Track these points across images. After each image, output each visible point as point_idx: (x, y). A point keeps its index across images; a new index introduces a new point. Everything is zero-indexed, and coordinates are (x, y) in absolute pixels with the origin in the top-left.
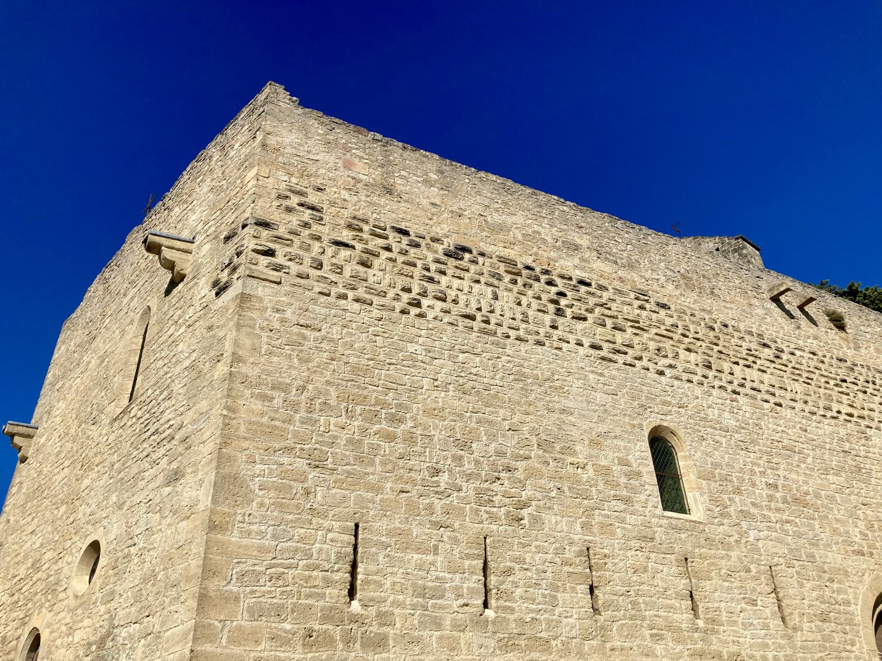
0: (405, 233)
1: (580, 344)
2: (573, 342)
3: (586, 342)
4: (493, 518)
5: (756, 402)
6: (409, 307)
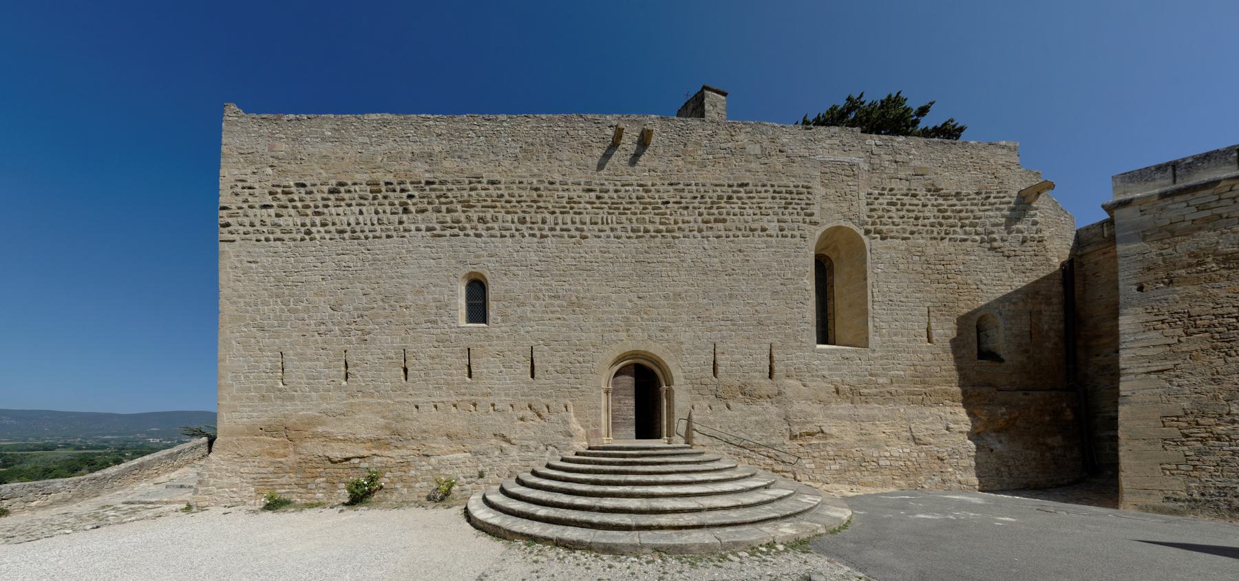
0: (303, 185)
1: (418, 230)
2: (247, 224)
3: (423, 227)
4: (350, 343)
5: (563, 239)
6: (945, 236)
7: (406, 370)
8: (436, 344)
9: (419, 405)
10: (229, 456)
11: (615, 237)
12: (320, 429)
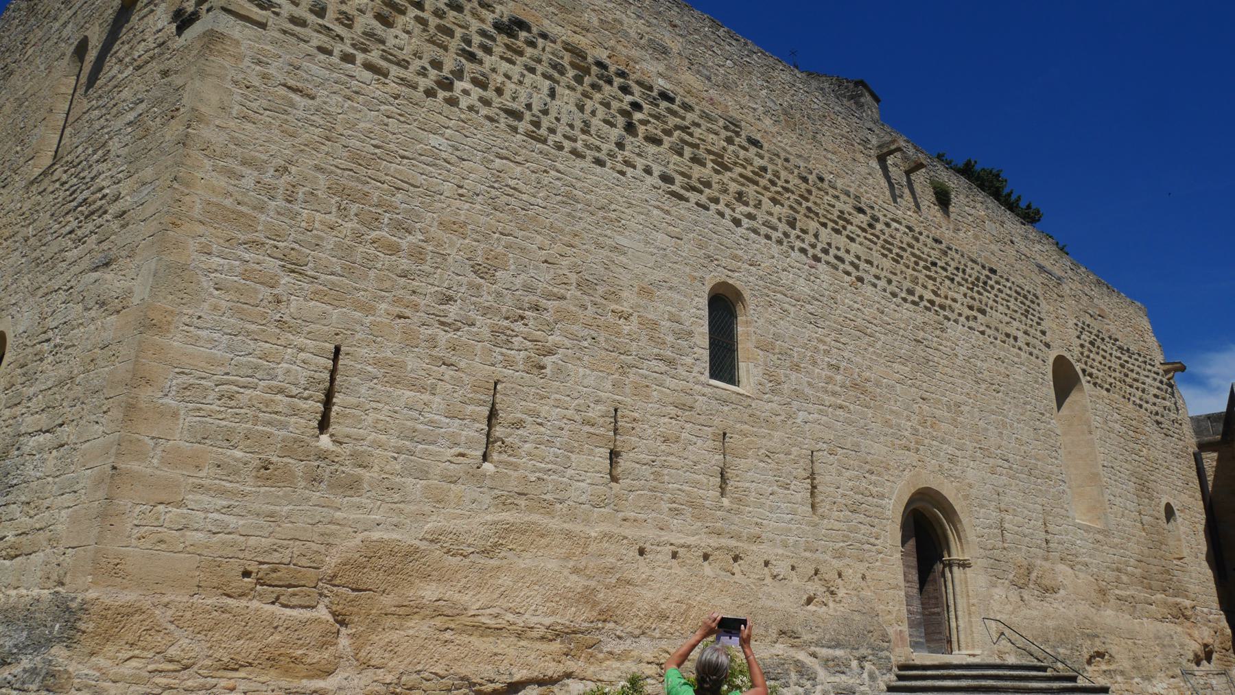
1: (648, 171)
2: (640, 167)
4: (509, 363)
7: (614, 455)
8: (673, 411)
9: (648, 547)
10: (134, 663)
11: (697, 204)
12: (429, 592)
